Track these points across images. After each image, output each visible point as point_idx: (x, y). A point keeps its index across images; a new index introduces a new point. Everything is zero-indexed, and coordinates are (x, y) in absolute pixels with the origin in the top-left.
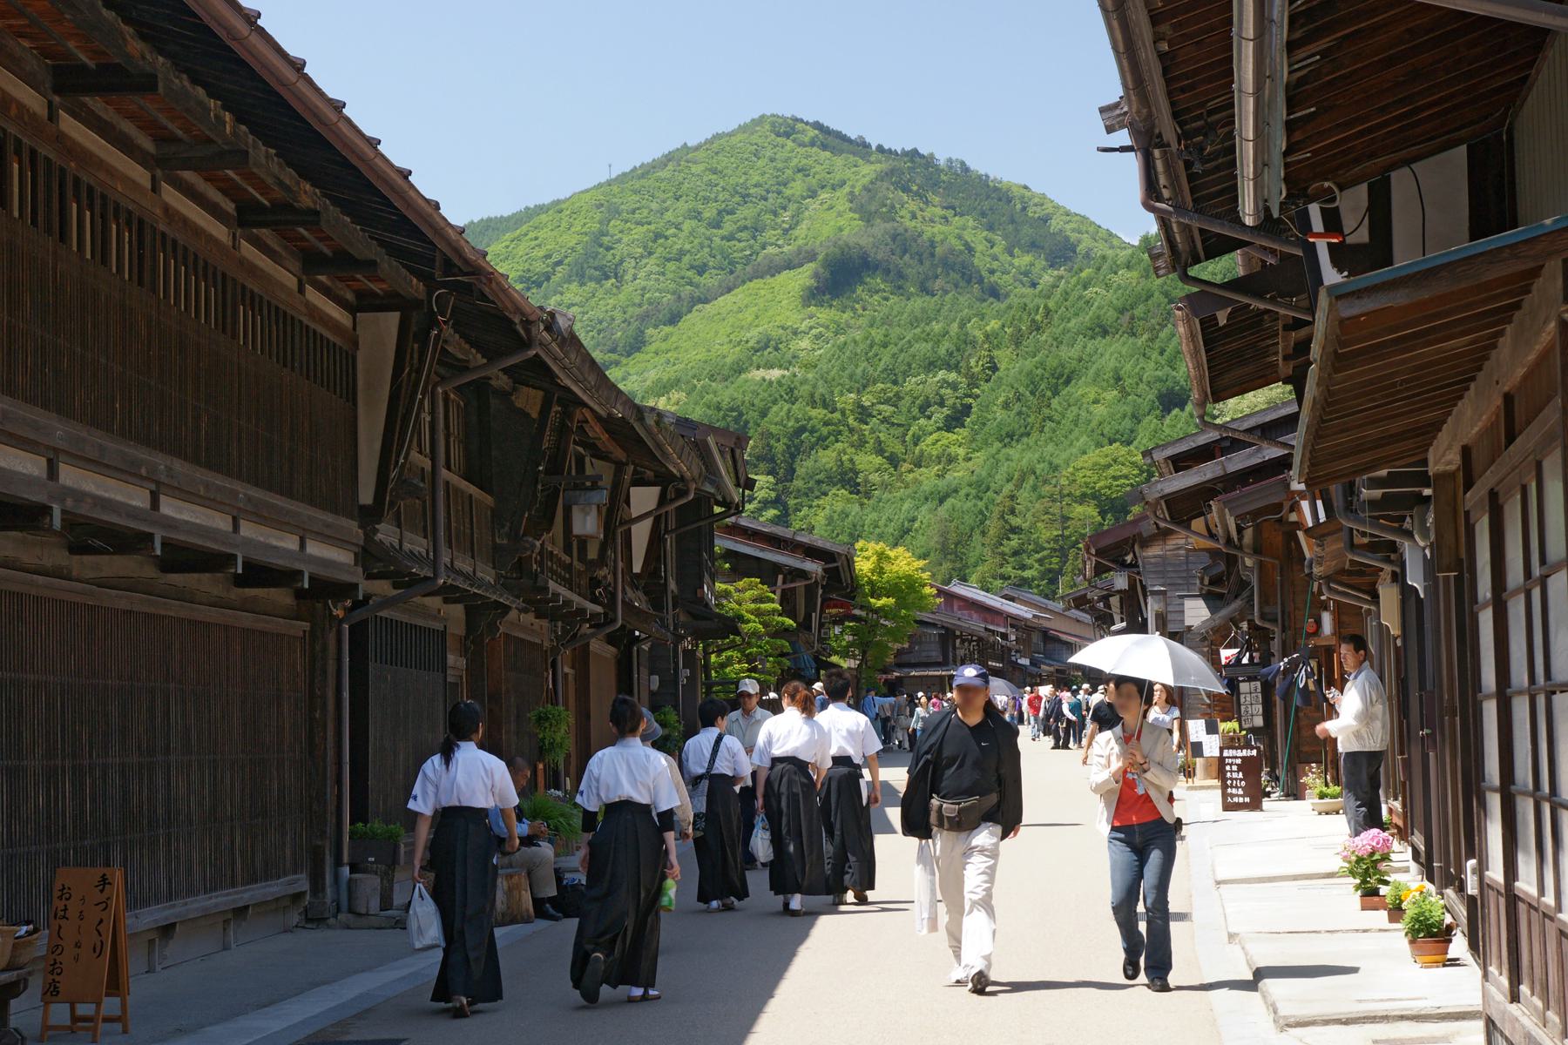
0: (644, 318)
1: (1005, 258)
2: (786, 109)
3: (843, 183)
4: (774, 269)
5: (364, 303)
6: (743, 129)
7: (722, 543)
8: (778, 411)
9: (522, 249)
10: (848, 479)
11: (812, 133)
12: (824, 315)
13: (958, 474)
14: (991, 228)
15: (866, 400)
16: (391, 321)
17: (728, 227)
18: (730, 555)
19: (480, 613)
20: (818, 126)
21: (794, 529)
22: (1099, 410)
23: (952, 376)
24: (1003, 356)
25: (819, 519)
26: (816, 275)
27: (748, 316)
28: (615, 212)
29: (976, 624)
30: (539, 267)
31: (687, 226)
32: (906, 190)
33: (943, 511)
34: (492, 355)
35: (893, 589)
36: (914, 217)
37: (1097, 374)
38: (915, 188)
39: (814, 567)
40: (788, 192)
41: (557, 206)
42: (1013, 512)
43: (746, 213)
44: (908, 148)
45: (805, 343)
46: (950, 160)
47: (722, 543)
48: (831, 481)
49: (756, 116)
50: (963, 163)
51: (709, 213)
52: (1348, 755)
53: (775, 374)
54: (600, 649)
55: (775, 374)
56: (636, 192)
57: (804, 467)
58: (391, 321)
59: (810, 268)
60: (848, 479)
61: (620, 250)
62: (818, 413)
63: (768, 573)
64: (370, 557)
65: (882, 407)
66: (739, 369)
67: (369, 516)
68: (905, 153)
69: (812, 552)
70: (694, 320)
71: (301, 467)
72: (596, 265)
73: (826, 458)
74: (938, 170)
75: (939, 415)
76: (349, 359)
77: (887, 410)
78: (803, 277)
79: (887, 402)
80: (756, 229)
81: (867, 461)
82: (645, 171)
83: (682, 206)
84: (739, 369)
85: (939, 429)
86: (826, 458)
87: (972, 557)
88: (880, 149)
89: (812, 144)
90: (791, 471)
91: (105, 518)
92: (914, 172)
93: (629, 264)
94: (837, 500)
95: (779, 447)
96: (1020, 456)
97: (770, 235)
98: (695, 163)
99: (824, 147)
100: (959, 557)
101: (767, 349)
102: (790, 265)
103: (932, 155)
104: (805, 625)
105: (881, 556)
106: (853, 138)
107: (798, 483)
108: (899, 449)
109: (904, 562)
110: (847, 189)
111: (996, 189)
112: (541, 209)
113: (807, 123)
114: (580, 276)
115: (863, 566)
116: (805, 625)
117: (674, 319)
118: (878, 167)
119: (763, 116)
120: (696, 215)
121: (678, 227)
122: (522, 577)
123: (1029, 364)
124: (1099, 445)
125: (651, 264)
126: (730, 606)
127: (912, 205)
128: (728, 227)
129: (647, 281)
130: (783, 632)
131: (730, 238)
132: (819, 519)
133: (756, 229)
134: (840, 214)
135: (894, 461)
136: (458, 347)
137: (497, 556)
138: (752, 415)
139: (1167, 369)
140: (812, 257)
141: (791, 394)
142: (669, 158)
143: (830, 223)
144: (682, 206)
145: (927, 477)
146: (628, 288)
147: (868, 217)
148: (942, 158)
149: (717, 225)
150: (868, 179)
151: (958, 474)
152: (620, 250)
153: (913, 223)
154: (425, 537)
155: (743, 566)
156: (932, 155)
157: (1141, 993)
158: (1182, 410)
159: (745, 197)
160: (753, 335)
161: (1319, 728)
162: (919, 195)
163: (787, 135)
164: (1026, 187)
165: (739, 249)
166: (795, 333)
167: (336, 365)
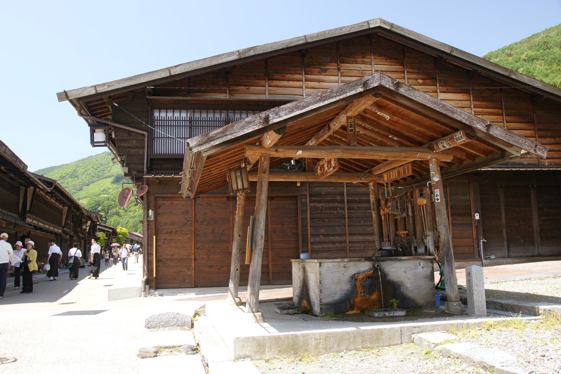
0: (83, 185)
4: (106, 178)
5: (64, 206)
6: (102, 153)
7: (98, 227)
8: (106, 202)
9: (61, 172)
10: (118, 214)
12: (115, 186)
13: (137, 214)
16: (67, 208)
17: (99, 170)
18: (99, 229)
19: (71, 237)
21: (107, 224)
25: (112, 221)
27: (101, 185)
28: (78, 166)
29: (136, 239)
30: (64, 175)
31: (91, 169)
33: (134, 220)
34: (77, 211)
35: (122, 234)
39: (111, 231)
41: (67, 165)
43: (102, 168)
45: (111, 190)
47: (98, 227)
48: (115, 214)
51: (95, 167)
53: (106, 196)
54: (83, 241)
55: (106, 196)
57: (110, 212)
58: (67, 208)
59: (113, 178)
60: (118, 214)
61: (78, 173)
62: (113, 203)
63: (104, 231)
64: (63, 231)
66: (99, 195)
67: (63, 227)
69: (111, 228)
70: (91, 186)
71: (58, 223)
72: (74, 175)
73: (114, 210)
76: (62, 211)
78: (112, 179)
80: (104, 171)
81: (121, 211)
82: (84, 160)
83: (90, 166)
84: (99, 195)
86: (114, 210)
87: (139, 227)
90: (108, 213)
93: (80, 175)
94: (115, 217)
95: (106, 208)
97: (106, 172)
100: (136, 227)
101: (105, 191)
102: (109, 177)
104: (109, 238)
105: (121, 229)
107: (109, 214)
108: (127, 209)
109: (125, 230)
112: (64, 165)
114: (71, 177)
115: (118, 230)
116: (109, 238)
117: (88, 185)
120: (93, 168)
122: (76, 233)
125: (84, 176)
126: (99, 236)
128: (99, 170)
129: (83, 178)
130: (106, 239)
132: (112, 221)
133: (104, 171)
135: (126, 211)
136: (73, 210)
137: (73, 231)
138: (101, 203)
140: (113, 176)
141: (108, 199)
142: (89, 157)
144: (90, 166)
145: (132, 214)
146: (80, 180)
149: (96, 169)
151: (137, 214)
152: (78, 173)
155: (101, 230)
157: (201, 348)
159: (102, 165)
160: (102, 189)
165: (100, 174)
167: (61, 212)
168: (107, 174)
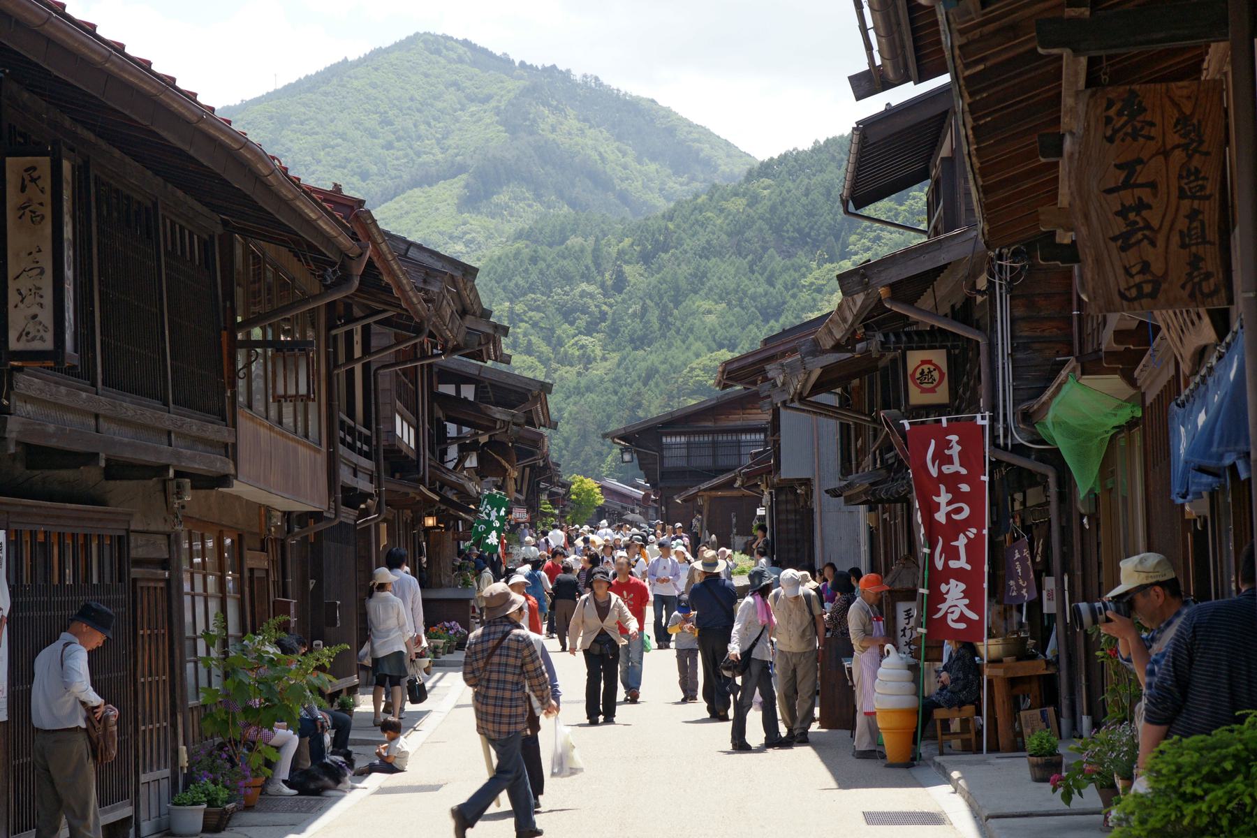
1: (634, 165)
2: (439, 29)
3: (488, 99)
4: (426, 179)
11: (461, 50)
13: (598, 371)
14: (619, 138)
15: (519, 308)
20: (466, 43)
22: (711, 319)
23: (591, 288)
24: (632, 271)
26: (467, 186)
32: (546, 104)
36: (553, 130)
37: (711, 289)
38: (555, 103)
40: (439, 105)
42: (639, 405)
44: (548, 65)
46: (585, 76)
49: (411, 34)
50: (597, 79)
52: (1049, 615)
56: (305, 105)
65: (531, 314)
68: (545, 69)
74: (575, 85)
75: (582, 322)
77: (536, 316)
79: (538, 309)
85: (580, 333)
88: (522, 64)
89: (461, 60)
91: (147, 458)
92: (549, 85)
96: (647, 358)
98: (356, 78)
99: (474, 64)
103: (569, 71)
106: (498, 54)
110: (493, 103)
111: (626, 103)
113: (457, 41)
118: (522, 83)
119: (417, 34)
121: (343, 136)
123: (653, 280)
124: (711, 350)
127: (551, 119)
131: (389, 146)
134: (487, 126)
139: (766, 286)
143: (480, 133)
147: (513, 130)
148: (577, 75)
150: (512, 95)
153: (553, 136)
154: (371, 482)
156: (569, 71)
158: (777, 321)
161: (404, 575)
162: (556, 110)
163: (438, 52)
164: (653, 101)
166: (451, 238)
168: (434, 156)
